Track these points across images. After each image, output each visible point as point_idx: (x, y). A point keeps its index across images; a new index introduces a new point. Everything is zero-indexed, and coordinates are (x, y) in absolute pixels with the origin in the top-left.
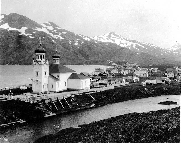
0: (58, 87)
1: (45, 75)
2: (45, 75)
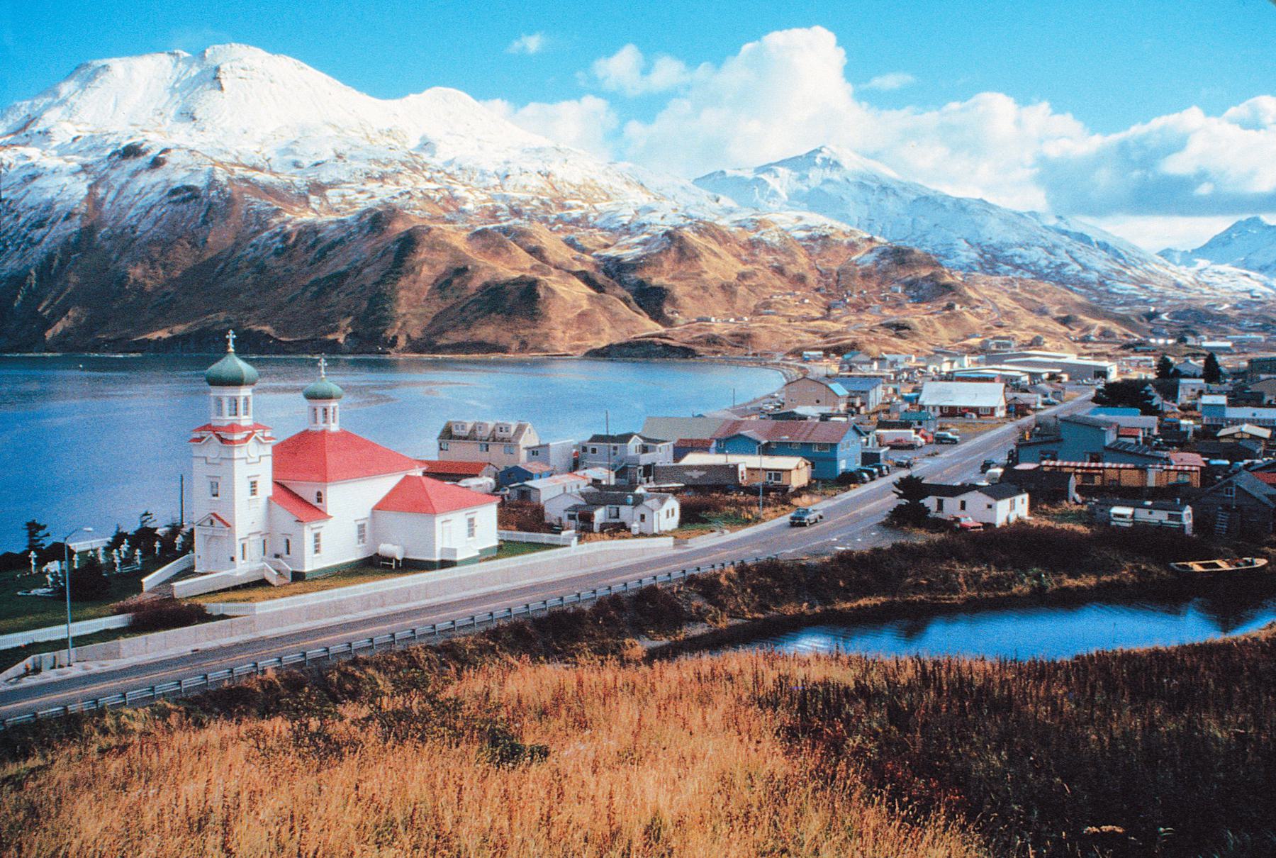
0: (317, 551)
1: (254, 492)
2: (254, 492)
